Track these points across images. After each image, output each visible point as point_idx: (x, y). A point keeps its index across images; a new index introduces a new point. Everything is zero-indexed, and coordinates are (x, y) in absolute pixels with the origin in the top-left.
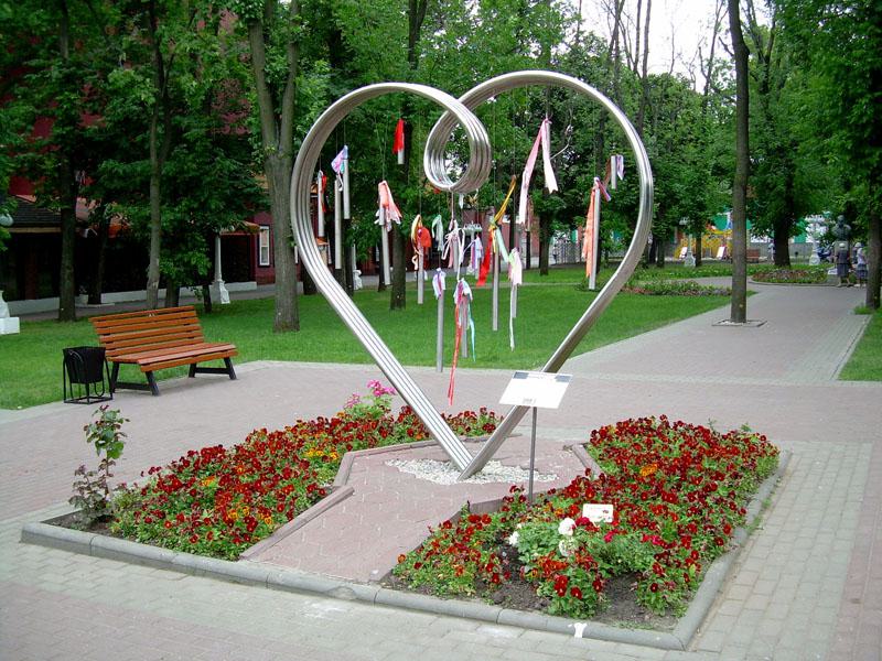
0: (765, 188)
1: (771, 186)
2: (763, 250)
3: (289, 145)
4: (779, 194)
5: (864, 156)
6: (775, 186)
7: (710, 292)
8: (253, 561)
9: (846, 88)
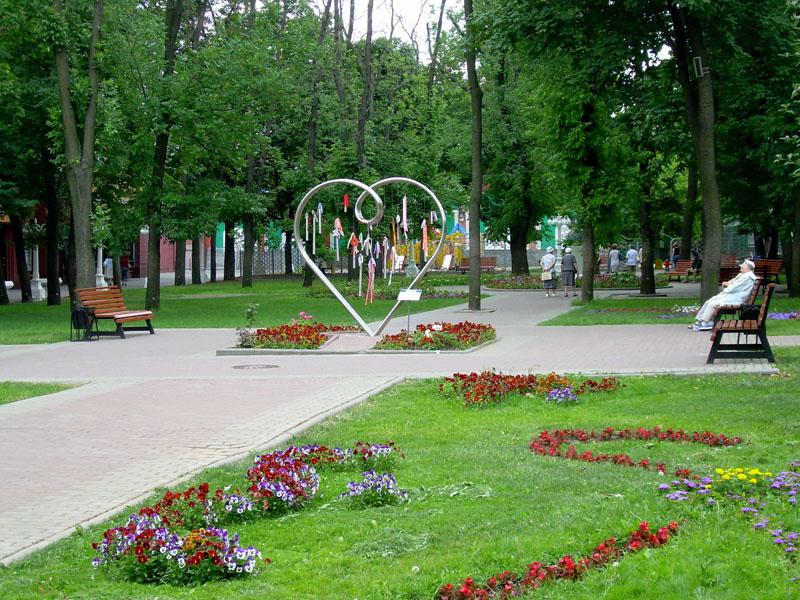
0: (500, 187)
1: (507, 185)
2: (500, 259)
3: (91, 157)
4: (517, 194)
5: (577, 174)
6: (511, 186)
7: (446, 296)
8: (322, 348)
9: (563, 118)
